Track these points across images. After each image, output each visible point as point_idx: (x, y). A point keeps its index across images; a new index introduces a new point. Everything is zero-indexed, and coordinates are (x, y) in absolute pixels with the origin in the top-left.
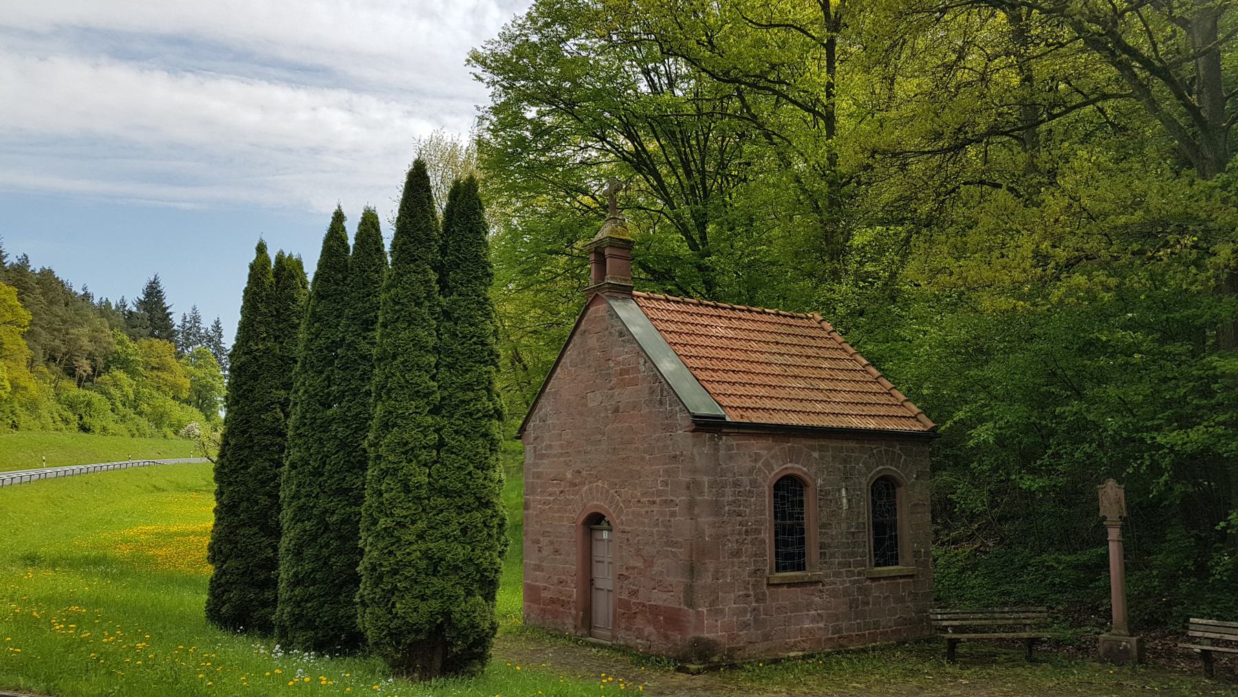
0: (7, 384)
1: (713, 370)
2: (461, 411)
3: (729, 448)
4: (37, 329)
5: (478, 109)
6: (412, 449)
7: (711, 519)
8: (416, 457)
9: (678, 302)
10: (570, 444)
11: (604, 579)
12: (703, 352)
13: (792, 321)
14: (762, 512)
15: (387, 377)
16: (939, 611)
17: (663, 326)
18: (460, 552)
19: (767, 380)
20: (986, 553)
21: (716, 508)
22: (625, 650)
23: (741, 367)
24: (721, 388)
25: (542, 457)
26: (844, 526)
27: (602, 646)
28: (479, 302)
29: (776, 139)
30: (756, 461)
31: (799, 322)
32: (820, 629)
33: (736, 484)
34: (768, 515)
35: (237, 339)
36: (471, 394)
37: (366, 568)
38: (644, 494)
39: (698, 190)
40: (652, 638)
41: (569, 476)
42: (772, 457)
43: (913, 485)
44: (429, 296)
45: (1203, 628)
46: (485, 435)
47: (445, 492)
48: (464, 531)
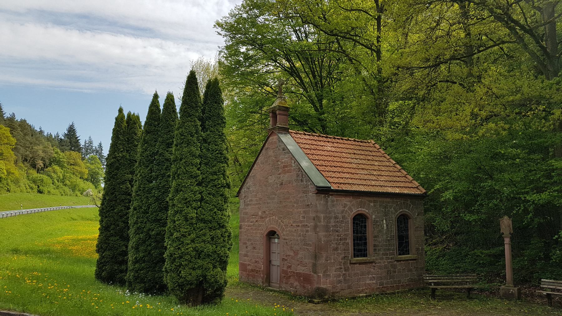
0: (5, 171)
1: (325, 166)
2: (211, 184)
3: (333, 201)
4: (19, 146)
5: (219, 47)
6: (189, 201)
7: (324, 233)
8: (191, 205)
9: (310, 135)
10: (260, 199)
11: (276, 261)
12: (321, 158)
13: (361, 144)
14: (347, 230)
15: (178, 169)
16: (428, 275)
17: (302, 146)
18: (210, 248)
19: (350, 170)
20: (449, 249)
21: (327, 228)
22: (285, 293)
23: (338, 164)
24: (329, 174)
25: (248, 205)
26: (385, 236)
27: (275, 291)
28: (219, 135)
29: (354, 61)
30: (345, 207)
31: (365, 144)
32: (373, 283)
33: (336, 218)
34: (350, 232)
35: (110, 151)
36: (216, 177)
37: (168, 256)
38: (294, 222)
39: (318, 84)
40: (298, 287)
41: (260, 213)
42: (352, 205)
43: (416, 218)
44: (197, 132)
45: (547, 284)
46: (222, 195)
47: (204, 221)
48: (212, 239)
